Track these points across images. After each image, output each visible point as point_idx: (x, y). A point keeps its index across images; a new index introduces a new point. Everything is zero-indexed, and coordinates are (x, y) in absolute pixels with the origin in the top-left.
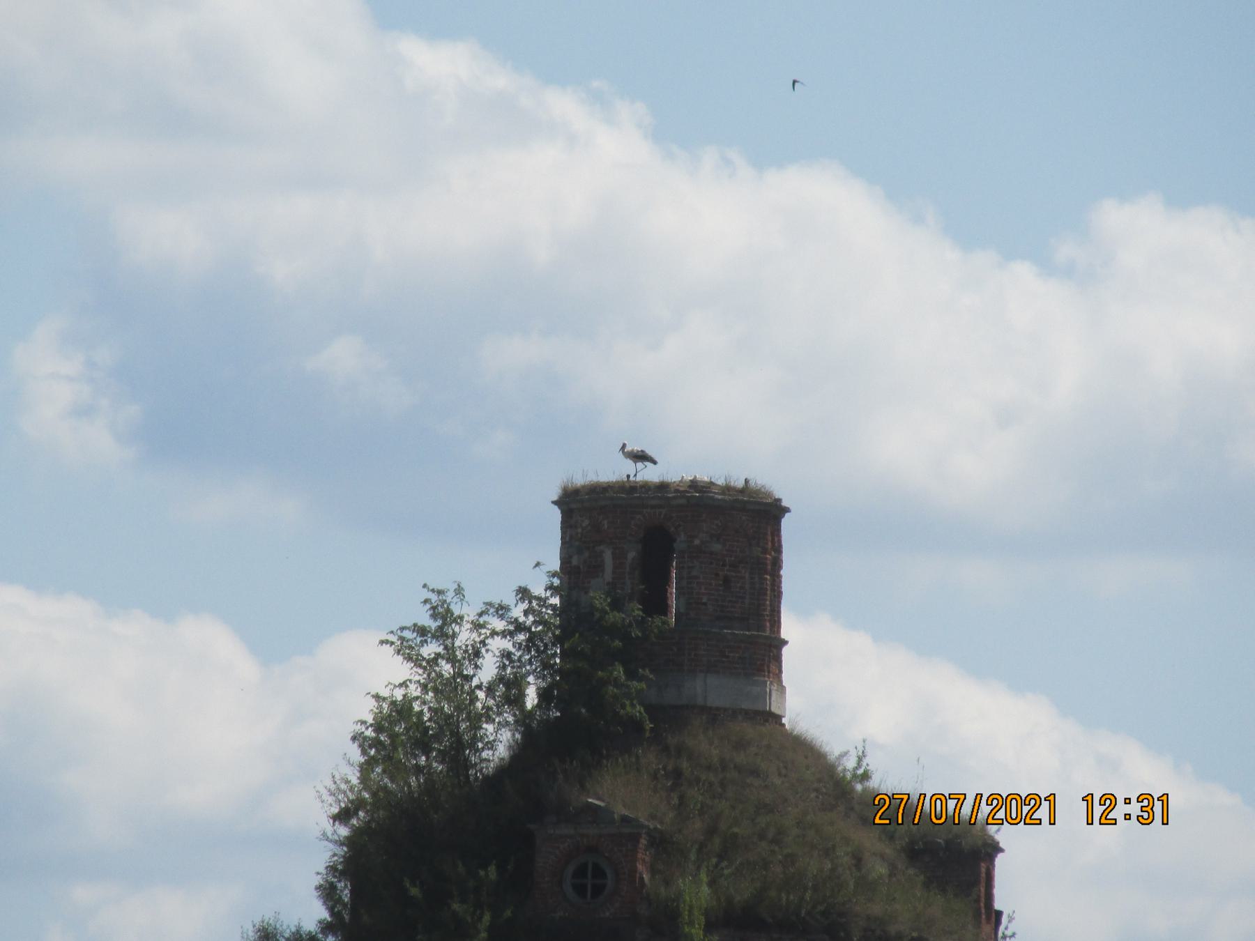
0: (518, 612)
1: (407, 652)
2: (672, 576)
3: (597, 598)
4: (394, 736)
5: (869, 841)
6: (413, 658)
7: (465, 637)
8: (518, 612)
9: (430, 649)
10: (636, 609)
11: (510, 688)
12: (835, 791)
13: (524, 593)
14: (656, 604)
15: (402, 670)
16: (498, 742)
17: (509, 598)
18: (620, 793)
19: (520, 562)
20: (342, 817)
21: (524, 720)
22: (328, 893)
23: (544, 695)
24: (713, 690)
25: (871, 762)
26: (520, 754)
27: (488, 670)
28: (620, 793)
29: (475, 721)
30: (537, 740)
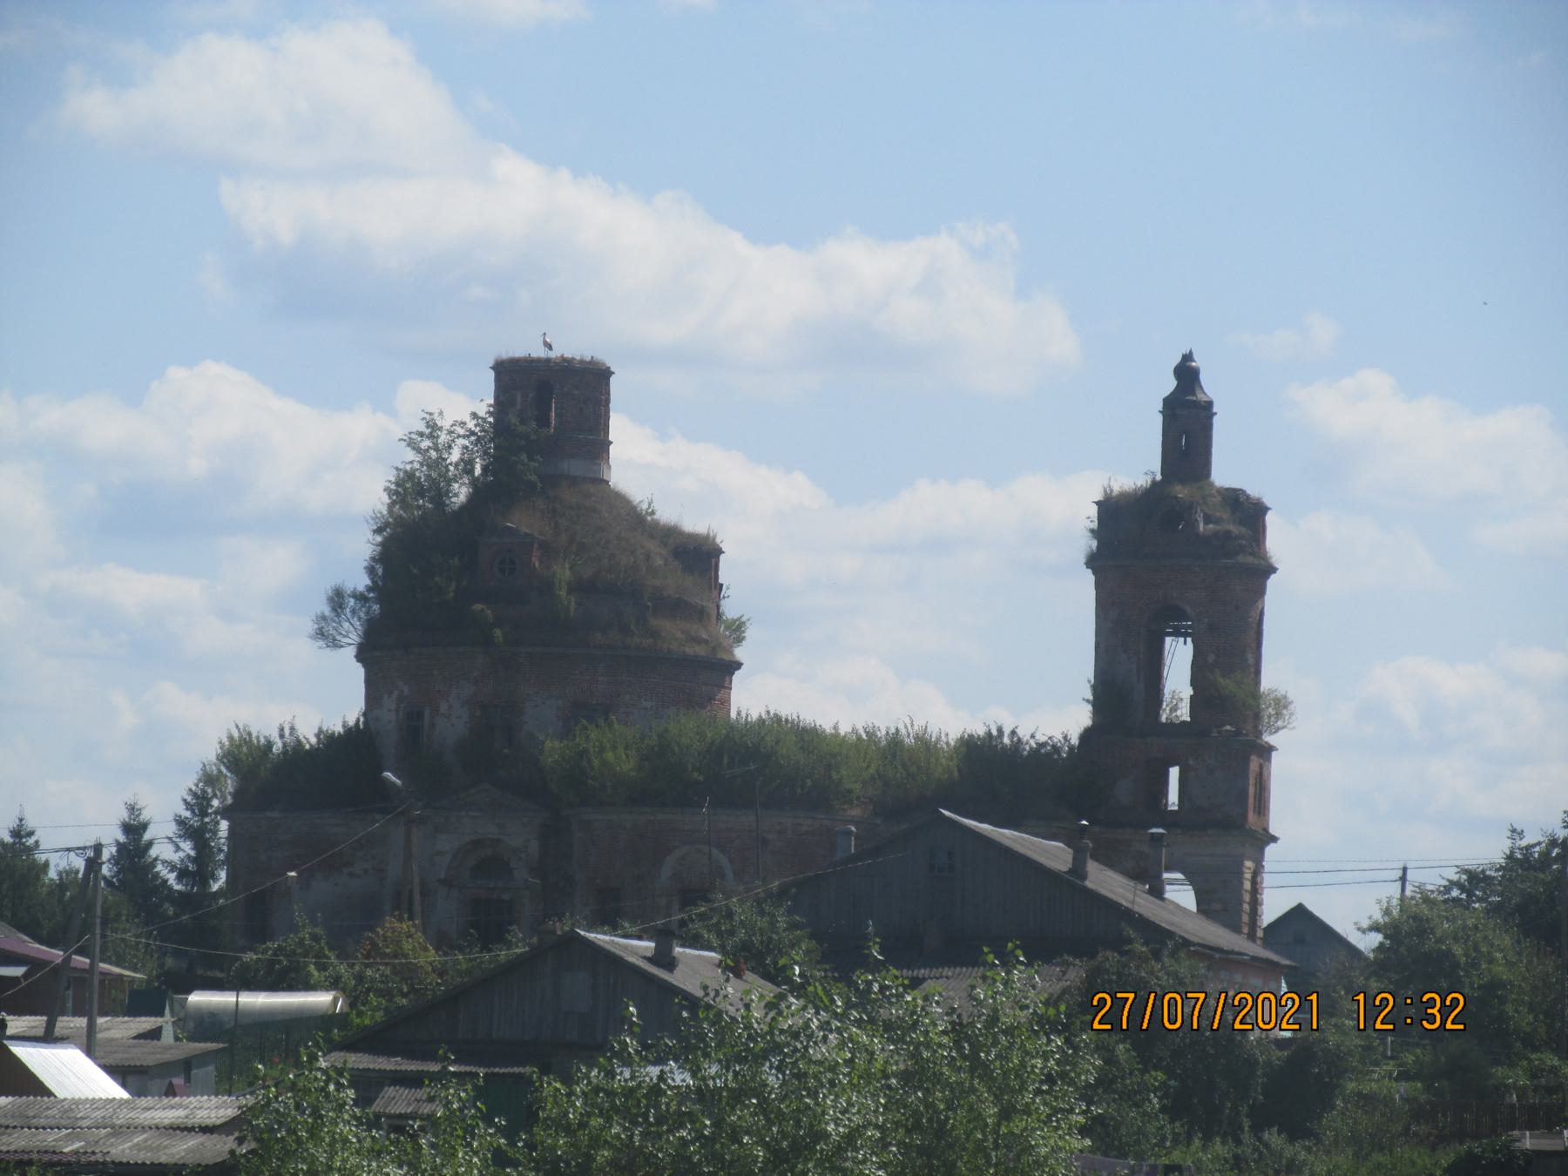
0: (471, 425)
1: (412, 444)
2: (550, 408)
3: (513, 419)
4: (406, 489)
5: (652, 546)
6: (418, 450)
7: (443, 438)
8: (471, 425)
9: (426, 444)
10: (534, 424)
11: (467, 465)
12: (638, 521)
13: (474, 415)
14: (543, 421)
15: (410, 455)
16: (461, 493)
17: (467, 419)
18: (523, 521)
19: (465, 403)
20: (378, 531)
21: (474, 482)
22: (371, 571)
23: (485, 469)
24: (574, 467)
25: (656, 506)
26: (471, 499)
27: (455, 456)
28: (523, 521)
29: (449, 482)
30: (479, 489)
